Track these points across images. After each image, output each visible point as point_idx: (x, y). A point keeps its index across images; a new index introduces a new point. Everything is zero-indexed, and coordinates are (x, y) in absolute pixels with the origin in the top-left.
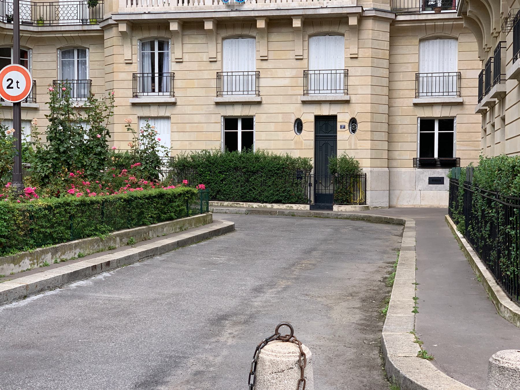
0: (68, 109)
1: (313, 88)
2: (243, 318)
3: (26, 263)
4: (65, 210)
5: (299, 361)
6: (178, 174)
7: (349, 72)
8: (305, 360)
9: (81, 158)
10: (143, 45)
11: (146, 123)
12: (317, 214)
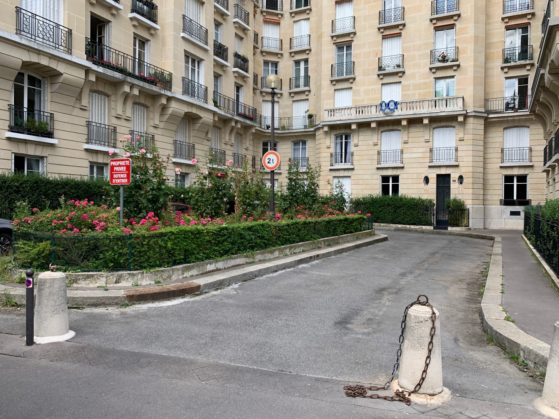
0: (297, 173)
1: (435, 158)
2: (395, 290)
3: (277, 254)
4: (296, 226)
5: (431, 317)
6: (355, 208)
7: (458, 148)
8: (435, 316)
9: (303, 199)
10: (336, 138)
11: (337, 180)
12: (438, 232)
